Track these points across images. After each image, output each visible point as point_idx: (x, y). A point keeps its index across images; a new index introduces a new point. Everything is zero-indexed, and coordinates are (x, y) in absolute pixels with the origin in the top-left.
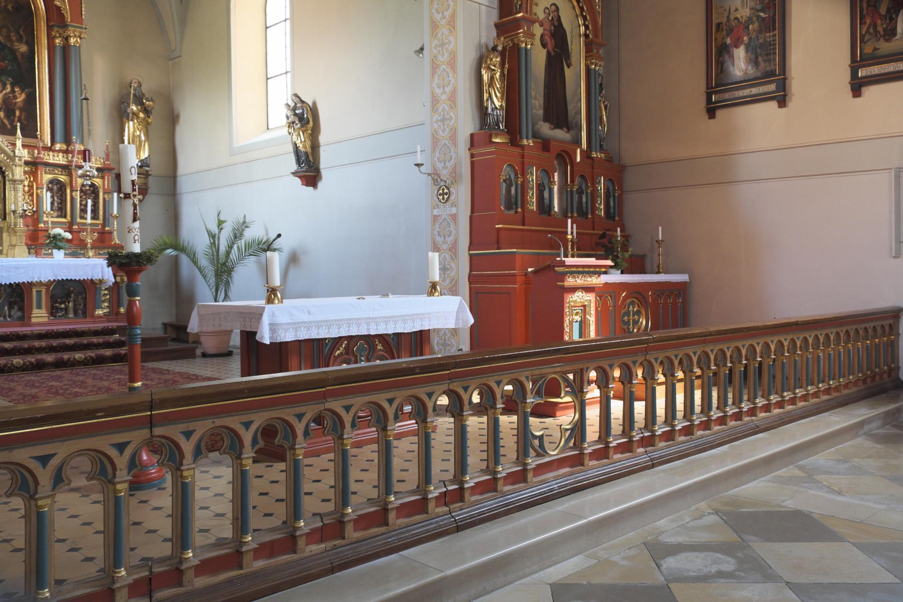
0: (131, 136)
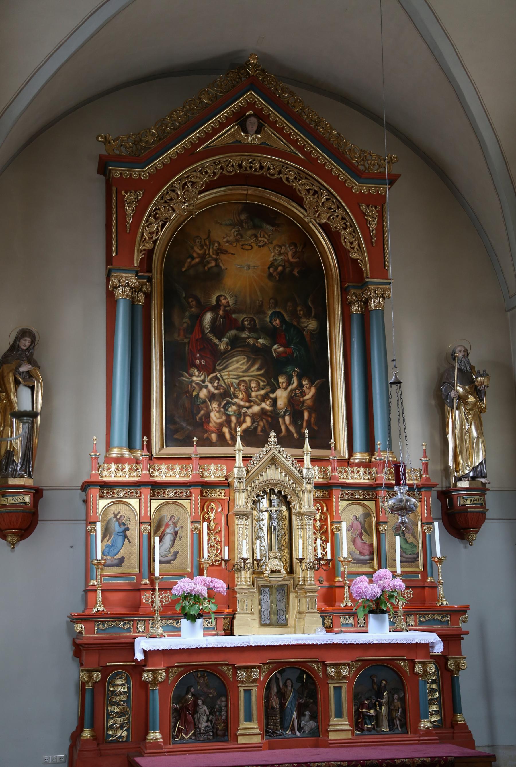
0: (457, 431)
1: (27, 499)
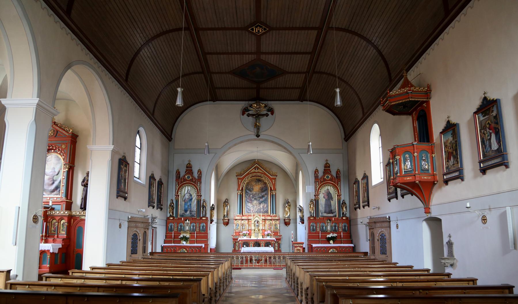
1: (227, 221)
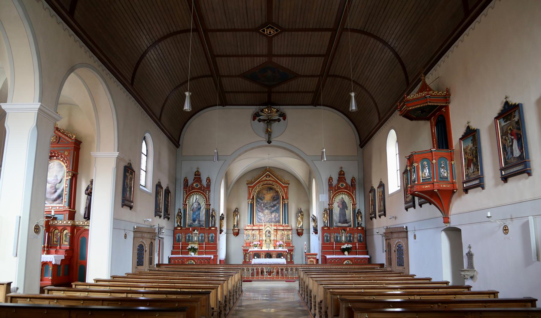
1: (237, 231)
